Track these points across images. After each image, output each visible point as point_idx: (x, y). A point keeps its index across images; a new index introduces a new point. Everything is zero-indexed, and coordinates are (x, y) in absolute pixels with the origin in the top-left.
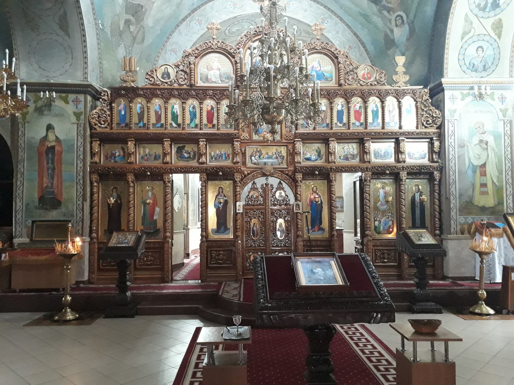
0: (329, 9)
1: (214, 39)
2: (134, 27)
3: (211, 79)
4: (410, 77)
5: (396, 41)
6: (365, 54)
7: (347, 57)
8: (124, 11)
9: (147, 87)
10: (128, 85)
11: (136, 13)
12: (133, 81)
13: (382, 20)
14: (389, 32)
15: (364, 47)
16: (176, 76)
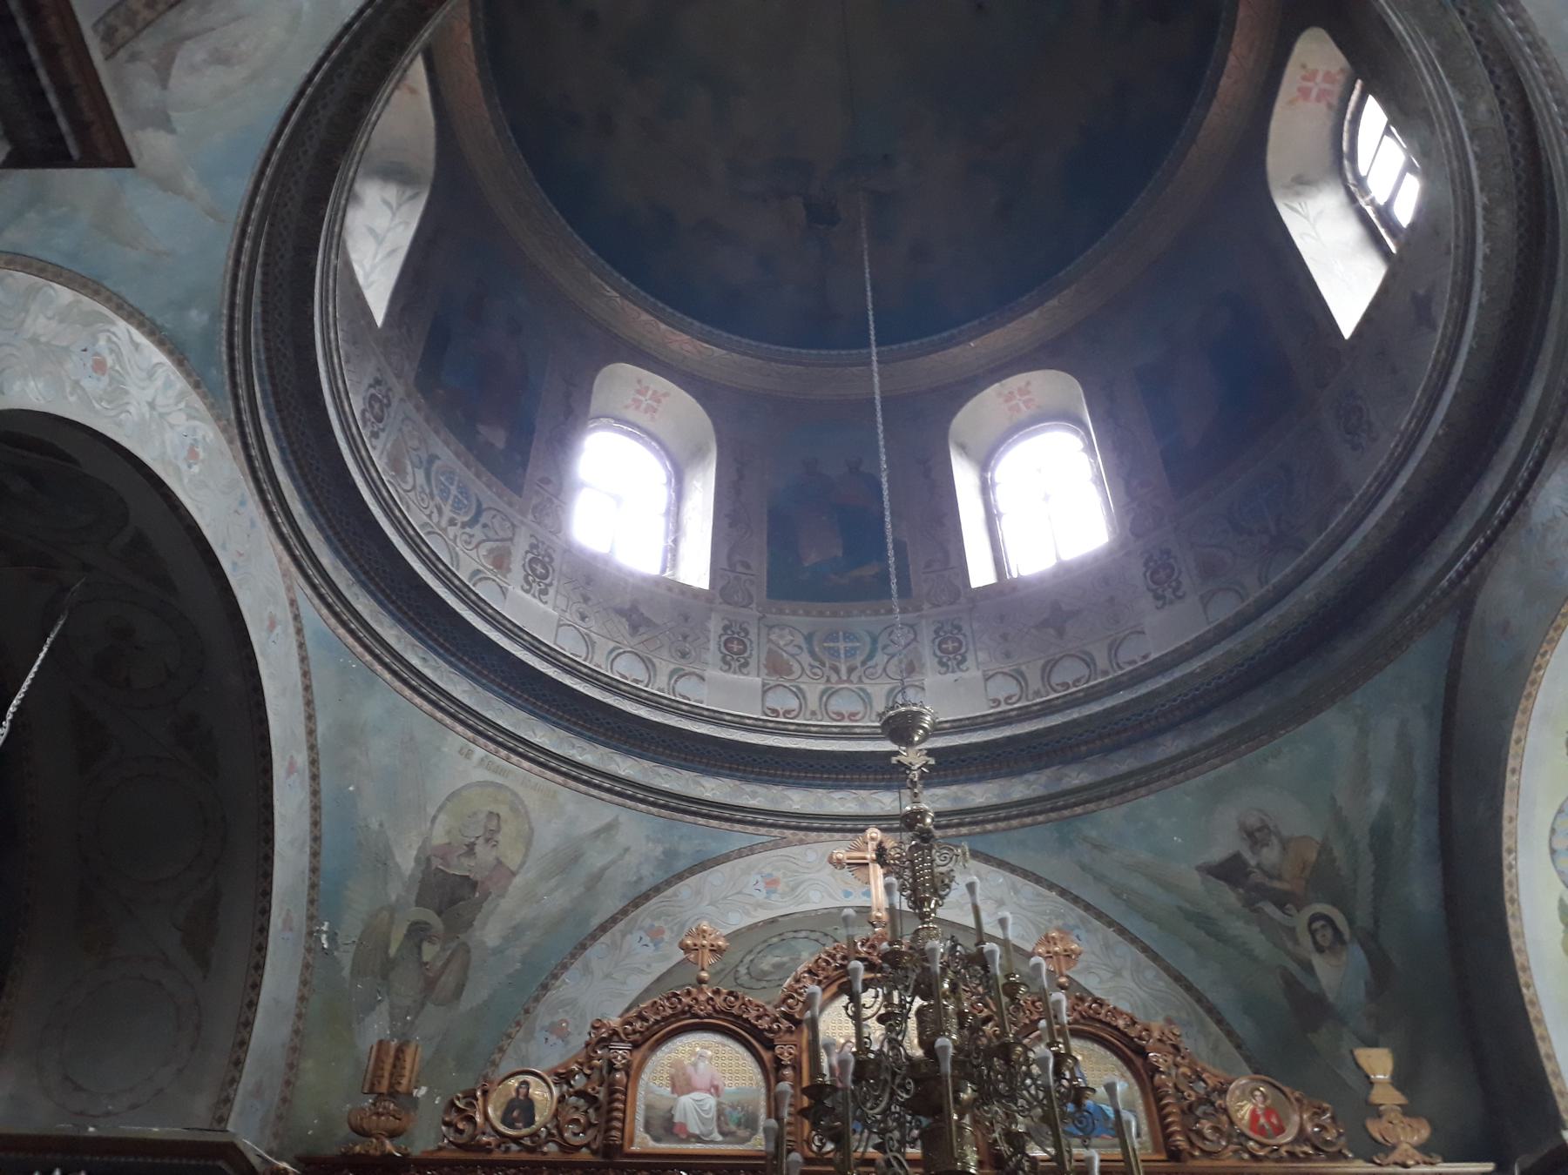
0: (1076, 900)
1: (701, 981)
2: (437, 948)
3: (683, 1126)
4: (1430, 1122)
5: (1331, 997)
6: (1227, 1046)
7: (1176, 1048)
8: (413, 898)
9: (444, 1155)
10: (370, 1147)
11: (453, 902)
12: (393, 1135)
13: (1262, 931)
14: (1293, 967)
15: (1220, 1022)
16: (556, 1115)
